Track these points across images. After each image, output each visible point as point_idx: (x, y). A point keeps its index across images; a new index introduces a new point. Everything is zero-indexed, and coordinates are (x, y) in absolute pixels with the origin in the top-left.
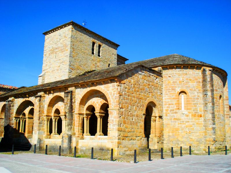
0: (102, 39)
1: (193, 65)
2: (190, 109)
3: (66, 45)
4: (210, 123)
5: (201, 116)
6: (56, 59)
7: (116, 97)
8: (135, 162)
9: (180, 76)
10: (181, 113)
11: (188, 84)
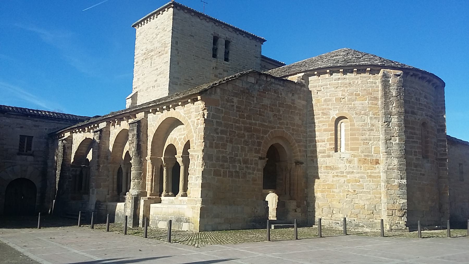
0: (232, 31)
1: (362, 68)
2: (357, 149)
3: (165, 44)
4: (394, 175)
5: (377, 162)
6: (152, 69)
7: (200, 129)
8: (382, 235)
9: (338, 89)
10: (339, 156)
11: (353, 103)
